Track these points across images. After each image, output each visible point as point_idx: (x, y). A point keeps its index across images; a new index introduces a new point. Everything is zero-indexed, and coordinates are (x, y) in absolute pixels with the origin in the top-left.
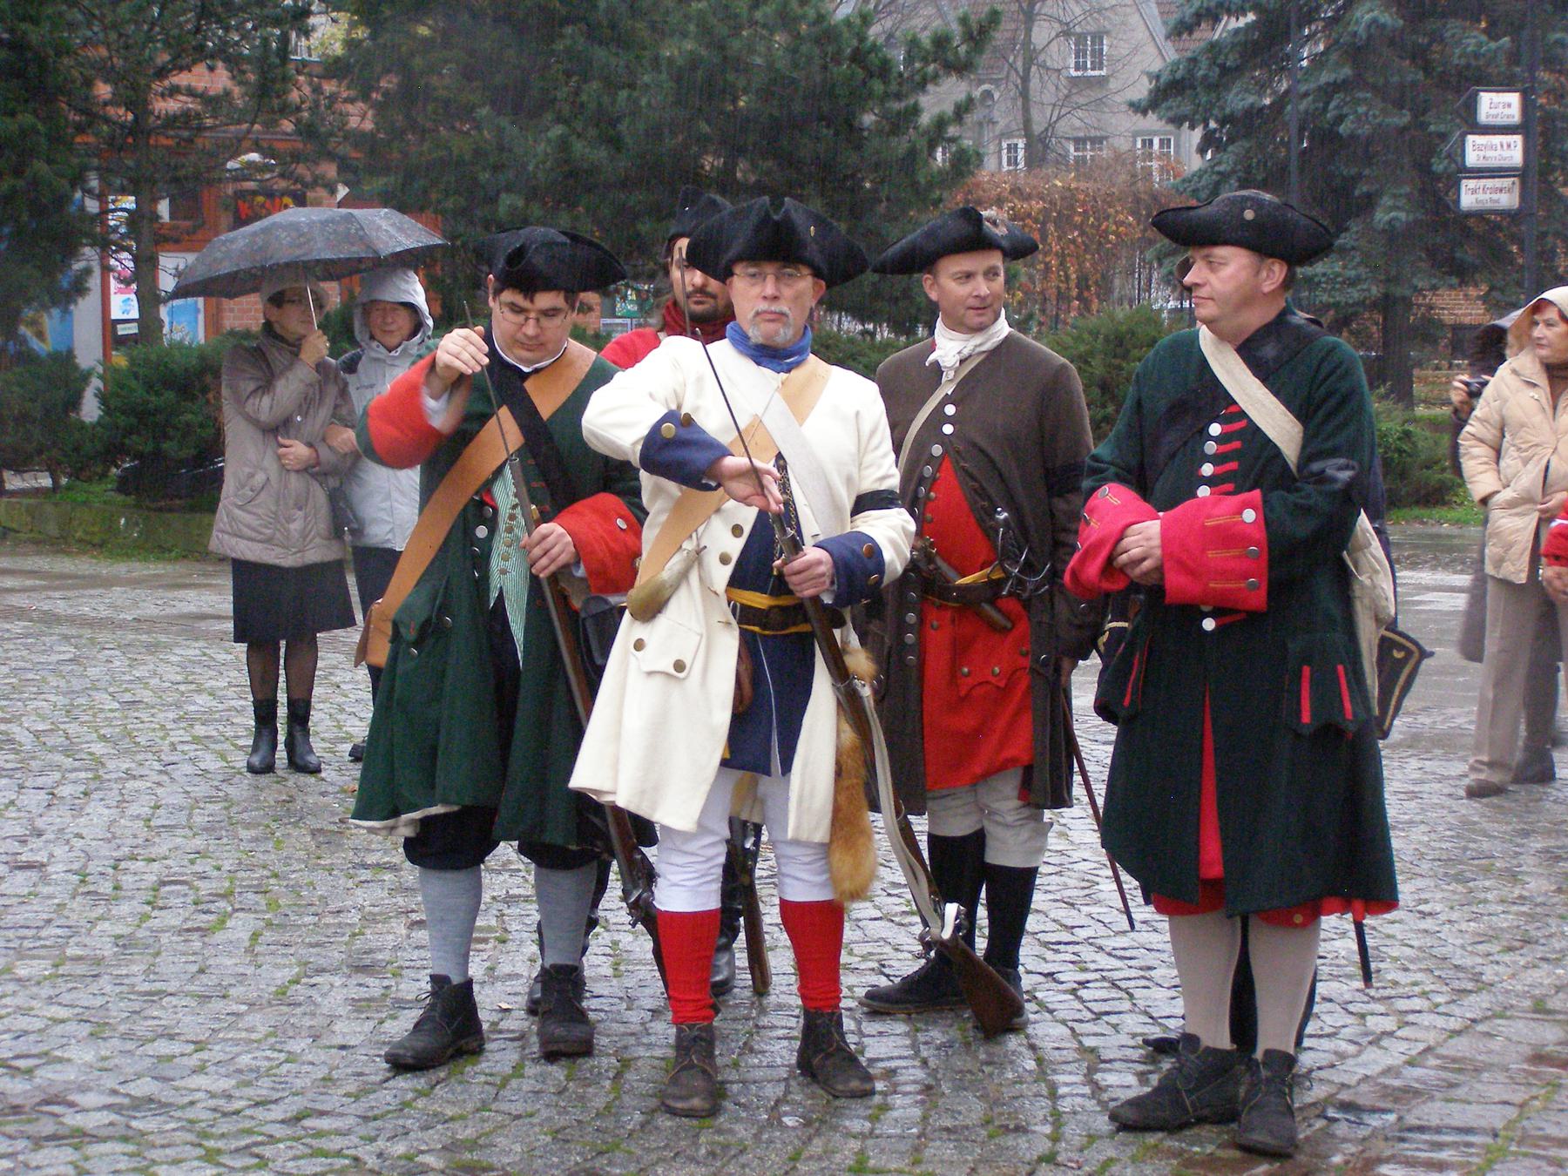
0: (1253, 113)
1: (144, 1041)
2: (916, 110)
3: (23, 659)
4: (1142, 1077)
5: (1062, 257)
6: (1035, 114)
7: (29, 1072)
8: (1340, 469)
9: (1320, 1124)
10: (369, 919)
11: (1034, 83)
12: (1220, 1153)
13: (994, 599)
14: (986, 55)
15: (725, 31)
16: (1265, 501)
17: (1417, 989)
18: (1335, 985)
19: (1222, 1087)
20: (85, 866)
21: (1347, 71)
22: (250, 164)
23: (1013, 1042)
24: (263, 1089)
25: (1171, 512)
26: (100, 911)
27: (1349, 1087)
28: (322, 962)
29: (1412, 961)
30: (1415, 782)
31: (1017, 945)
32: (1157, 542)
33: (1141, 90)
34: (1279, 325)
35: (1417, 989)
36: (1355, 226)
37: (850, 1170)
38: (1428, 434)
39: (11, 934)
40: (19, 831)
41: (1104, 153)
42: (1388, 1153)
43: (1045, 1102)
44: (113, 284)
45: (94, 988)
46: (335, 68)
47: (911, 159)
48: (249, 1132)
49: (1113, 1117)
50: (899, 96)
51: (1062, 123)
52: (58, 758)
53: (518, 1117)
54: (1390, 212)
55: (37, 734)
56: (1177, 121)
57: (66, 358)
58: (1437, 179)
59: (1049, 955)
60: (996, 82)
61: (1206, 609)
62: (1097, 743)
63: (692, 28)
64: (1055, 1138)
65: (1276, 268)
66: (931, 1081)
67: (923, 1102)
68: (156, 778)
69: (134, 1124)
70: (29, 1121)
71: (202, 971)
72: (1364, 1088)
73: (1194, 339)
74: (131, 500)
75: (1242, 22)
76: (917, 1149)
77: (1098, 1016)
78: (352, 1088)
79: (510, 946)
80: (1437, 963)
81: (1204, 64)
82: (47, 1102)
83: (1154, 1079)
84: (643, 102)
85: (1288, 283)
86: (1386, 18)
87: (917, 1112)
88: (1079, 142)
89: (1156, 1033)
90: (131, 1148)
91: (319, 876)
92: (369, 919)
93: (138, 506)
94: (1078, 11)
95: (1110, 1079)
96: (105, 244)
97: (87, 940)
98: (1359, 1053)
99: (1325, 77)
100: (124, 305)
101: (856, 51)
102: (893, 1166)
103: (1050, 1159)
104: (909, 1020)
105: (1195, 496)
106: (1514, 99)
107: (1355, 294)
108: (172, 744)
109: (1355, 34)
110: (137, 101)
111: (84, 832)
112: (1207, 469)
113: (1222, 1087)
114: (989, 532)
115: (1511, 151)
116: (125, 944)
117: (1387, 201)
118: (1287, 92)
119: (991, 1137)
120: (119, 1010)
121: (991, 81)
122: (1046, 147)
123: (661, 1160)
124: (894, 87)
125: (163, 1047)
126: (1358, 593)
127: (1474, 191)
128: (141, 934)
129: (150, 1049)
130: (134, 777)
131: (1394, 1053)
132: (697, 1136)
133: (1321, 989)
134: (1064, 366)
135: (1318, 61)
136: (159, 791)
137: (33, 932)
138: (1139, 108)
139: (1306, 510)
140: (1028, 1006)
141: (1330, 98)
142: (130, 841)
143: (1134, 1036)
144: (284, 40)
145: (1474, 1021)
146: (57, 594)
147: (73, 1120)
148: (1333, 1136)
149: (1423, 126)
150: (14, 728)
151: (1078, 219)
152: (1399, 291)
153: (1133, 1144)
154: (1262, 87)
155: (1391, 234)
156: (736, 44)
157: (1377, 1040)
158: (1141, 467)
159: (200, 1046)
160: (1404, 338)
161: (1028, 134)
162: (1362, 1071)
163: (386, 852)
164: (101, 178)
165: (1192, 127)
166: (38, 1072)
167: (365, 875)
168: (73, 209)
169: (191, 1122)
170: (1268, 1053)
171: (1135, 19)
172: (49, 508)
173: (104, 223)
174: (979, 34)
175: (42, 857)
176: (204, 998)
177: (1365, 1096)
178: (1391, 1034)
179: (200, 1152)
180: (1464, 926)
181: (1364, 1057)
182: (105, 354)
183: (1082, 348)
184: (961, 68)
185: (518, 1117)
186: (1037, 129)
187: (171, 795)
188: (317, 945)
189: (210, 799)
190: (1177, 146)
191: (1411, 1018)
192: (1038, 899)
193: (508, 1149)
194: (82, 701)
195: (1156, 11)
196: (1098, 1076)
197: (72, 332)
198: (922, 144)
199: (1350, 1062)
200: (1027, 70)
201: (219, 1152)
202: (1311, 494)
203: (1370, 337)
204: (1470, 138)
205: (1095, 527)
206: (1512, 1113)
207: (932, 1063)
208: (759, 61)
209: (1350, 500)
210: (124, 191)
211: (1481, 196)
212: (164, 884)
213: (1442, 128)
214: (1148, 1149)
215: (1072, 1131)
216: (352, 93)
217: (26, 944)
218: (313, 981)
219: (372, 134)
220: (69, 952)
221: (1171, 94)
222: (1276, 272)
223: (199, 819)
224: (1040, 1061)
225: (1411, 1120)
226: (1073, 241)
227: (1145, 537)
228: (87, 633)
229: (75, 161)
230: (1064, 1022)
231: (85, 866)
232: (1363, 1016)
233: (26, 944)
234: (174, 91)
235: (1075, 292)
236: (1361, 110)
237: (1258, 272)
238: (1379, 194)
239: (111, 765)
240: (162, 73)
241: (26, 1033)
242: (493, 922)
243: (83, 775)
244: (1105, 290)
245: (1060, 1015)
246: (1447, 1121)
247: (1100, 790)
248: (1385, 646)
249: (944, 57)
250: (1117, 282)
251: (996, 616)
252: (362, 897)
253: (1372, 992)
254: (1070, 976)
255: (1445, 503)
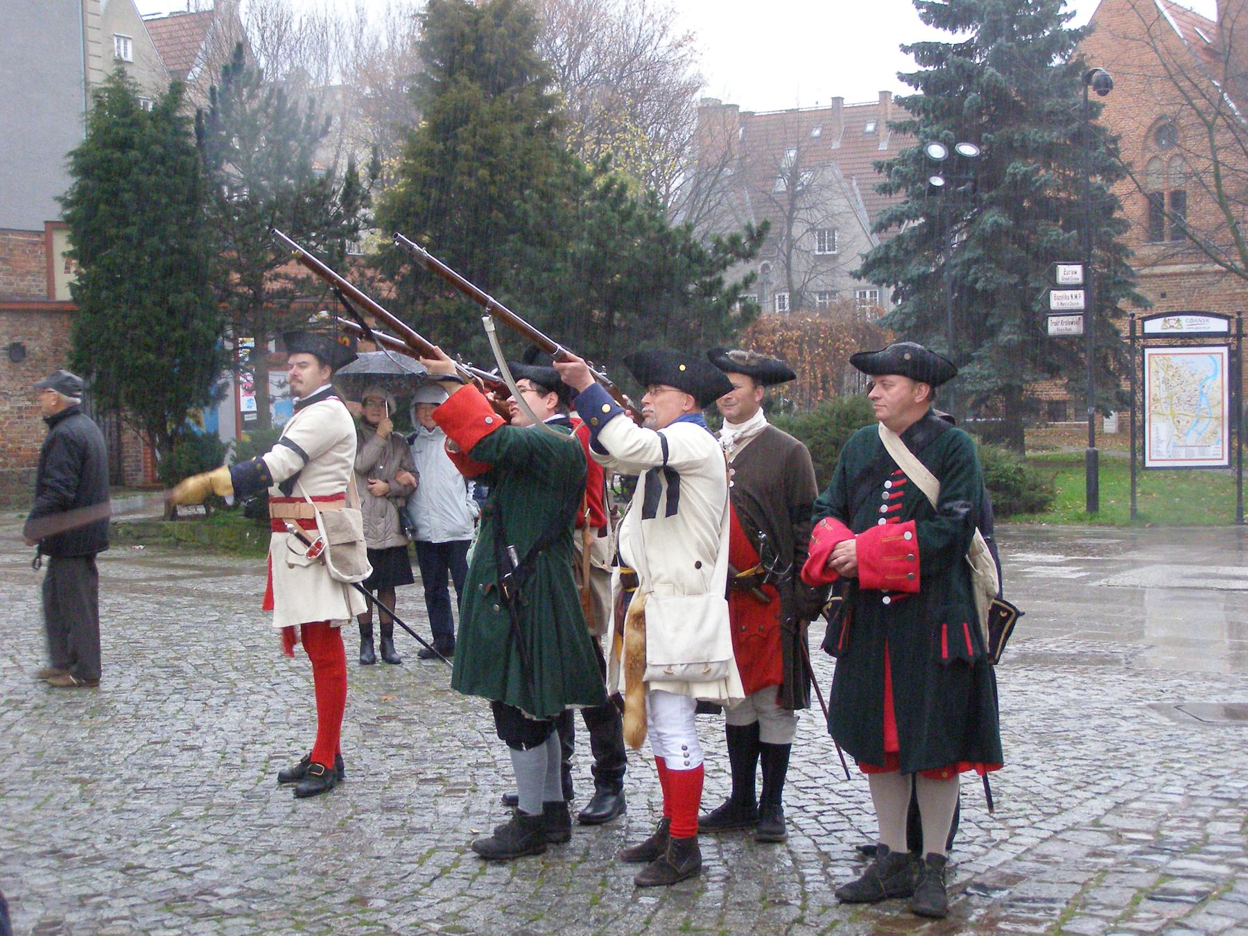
0: (924, 277)
1: (259, 855)
2: (720, 282)
3: (188, 620)
4: (856, 870)
5: (812, 363)
6: (795, 278)
7: (191, 874)
8: (961, 506)
9: (962, 897)
10: (394, 779)
11: (794, 259)
12: (904, 916)
13: (759, 586)
14: (765, 245)
15: (605, 236)
16: (918, 527)
17: (1022, 813)
18: (972, 811)
19: (902, 876)
20: (225, 748)
21: (980, 252)
22: (323, 319)
23: (778, 849)
24: (330, 882)
25: (864, 534)
26: (234, 775)
27: (979, 874)
28: (367, 806)
29: (1019, 796)
30: (1022, 684)
31: (780, 790)
32: (854, 552)
33: (857, 265)
34: (925, 421)
35: (1022, 813)
36: (987, 344)
37: (680, 929)
38: (1032, 469)
39: (180, 790)
40: (186, 727)
41: (837, 301)
42: (1004, 914)
43: (798, 886)
44: (242, 391)
45: (229, 823)
46: (373, 262)
47: (719, 311)
48: (322, 911)
49: (837, 895)
50: (710, 274)
51: (811, 283)
52: (209, 681)
53: (483, 899)
54: (1008, 335)
55: (196, 667)
56: (879, 283)
57: (213, 437)
58: (1035, 317)
59: (801, 795)
60: (771, 259)
61: (884, 591)
62: (823, 667)
63: (585, 235)
64: (803, 908)
65: (923, 388)
66: (728, 873)
67: (724, 887)
68: (267, 693)
69: (253, 906)
70: (190, 906)
71: (294, 812)
72: (989, 874)
73: (875, 433)
74: (254, 521)
75: (916, 223)
76: (721, 916)
77: (830, 832)
78: (383, 883)
79: (479, 794)
80: (1033, 797)
81: (894, 248)
82: (201, 893)
83: (863, 871)
84: (557, 279)
85: (931, 396)
86: (1002, 220)
87: (720, 893)
88: (822, 294)
89: (864, 842)
90: (251, 921)
91: (365, 752)
92: (394, 779)
93: (257, 525)
94: (819, 216)
95: (837, 871)
96: (236, 368)
97: (225, 794)
98: (986, 853)
99: (967, 255)
100: (248, 403)
101: (684, 247)
102: (706, 926)
103: (800, 921)
104: (717, 836)
105: (877, 524)
106: (1078, 268)
107: (987, 385)
108: (277, 672)
109: (983, 230)
110: (254, 282)
111: (224, 727)
112: (884, 508)
113: (902, 876)
114: (755, 544)
115: (1077, 300)
116: (248, 795)
117: (1006, 328)
118: (944, 264)
119: (765, 908)
120: (244, 837)
121: (769, 259)
122: (802, 297)
123: (567, 925)
124: (707, 268)
125: (269, 859)
126: (975, 580)
127: (1056, 324)
128: (258, 789)
129: (262, 860)
130: (254, 693)
131: (1007, 853)
132: (588, 909)
133: (962, 814)
134: (799, 446)
135: (963, 245)
136: (269, 701)
137: (192, 789)
138: (856, 275)
139: (942, 532)
140: (787, 827)
141: (970, 268)
142: (251, 732)
143: (851, 844)
144: (343, 245)
145: (1055, 832)
146: (209, 580)
147: (217, 905)
148: (970, 904)
149: (1025, 283)
150: (183, 663)
151: (821, 341)
152: (1016, 382)
153: (849, 910)
154: (929, 261)
155: (1008, 350)
156: (612, 244)
157: (997, 845)
158: (846, 507)
159: (293, 858)
160: (1014, 416)
161: (791, 291)
162: (988, 864)
163: (404, 737)
164: (234, 330)
165: (888, 286)
166: (196, 875)
167: (392, 751)
168: (217, 348)
169: (286, 904)
170: (930, 855)
171: (854, 221)
172: (205, 528)
173: (236, 355)
174: (758, 236)
175: (199, 743)
176: (295, 829)
177: (989, 880)
178: (1005, 841)
179: (291, 923)
180: (1050, 773)
181: (990, 855)
182: (238, 433)
183: (823, 421)
184: (749, 256)
185: (483, 899)
186: (796, 287)
187: (276, 704)
188: (364, 794)
189: (298, 705)
190: (881, 298)
191: (1018, 831)
192: (792, 759)
193: (477, 917)
194: (224, 646)
195: (866, 215)
196: (829, 869)
197: (217, 419)
198: (724, 302)
199: (981, 858)
200: (789, 253)
201: (303, 923)
202: (946, 523)
203: (997, 410)
204: (1053, 292)
205: (817, 543)
206: (1078, 889)
207: (731, 863)
208: (626, 254)
209: (967, 527)
210: (247, 336)
211: (1060, 327)
212: (271, 758)
213: (1037, 285)
214: (858, 914)
215: (813, 904)
216: (383, 276)
217: (190, 796)
218: (362, 816)
219: (395, 301)
220: (215, 801)
221: (877, 267)
222: (924, 390)
223: (293, 718)
224: (794, 861)
225: (1017, 894)
226: (818, 354)
227: (847, 549)
228: (226, 603)
229: (219, 319)
230: (809, 837)
231: (225, 748)
232: (988, 830)
233: (190, 796)
234: (277, 277)
235: (820, 385)
236: (989, 274)
237: (913, 390)
238: (1001, 325)
239: (241, 685)
240: (270, 266)
241: (188, 851)
242: (469, 779)
243: (224, 692)
244: (839, 384)
245: (807, 832)
246: (1038, 894)
247: (827, 698)
248: (995, 610)
249: (735, 249)
250: (846, 378)
251: (760, 594)
252: (392, 765)
253: (995, 815)
254: (814, 808)
255: (1044, 511)
